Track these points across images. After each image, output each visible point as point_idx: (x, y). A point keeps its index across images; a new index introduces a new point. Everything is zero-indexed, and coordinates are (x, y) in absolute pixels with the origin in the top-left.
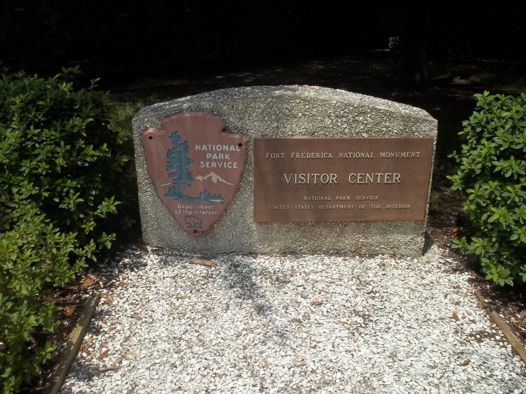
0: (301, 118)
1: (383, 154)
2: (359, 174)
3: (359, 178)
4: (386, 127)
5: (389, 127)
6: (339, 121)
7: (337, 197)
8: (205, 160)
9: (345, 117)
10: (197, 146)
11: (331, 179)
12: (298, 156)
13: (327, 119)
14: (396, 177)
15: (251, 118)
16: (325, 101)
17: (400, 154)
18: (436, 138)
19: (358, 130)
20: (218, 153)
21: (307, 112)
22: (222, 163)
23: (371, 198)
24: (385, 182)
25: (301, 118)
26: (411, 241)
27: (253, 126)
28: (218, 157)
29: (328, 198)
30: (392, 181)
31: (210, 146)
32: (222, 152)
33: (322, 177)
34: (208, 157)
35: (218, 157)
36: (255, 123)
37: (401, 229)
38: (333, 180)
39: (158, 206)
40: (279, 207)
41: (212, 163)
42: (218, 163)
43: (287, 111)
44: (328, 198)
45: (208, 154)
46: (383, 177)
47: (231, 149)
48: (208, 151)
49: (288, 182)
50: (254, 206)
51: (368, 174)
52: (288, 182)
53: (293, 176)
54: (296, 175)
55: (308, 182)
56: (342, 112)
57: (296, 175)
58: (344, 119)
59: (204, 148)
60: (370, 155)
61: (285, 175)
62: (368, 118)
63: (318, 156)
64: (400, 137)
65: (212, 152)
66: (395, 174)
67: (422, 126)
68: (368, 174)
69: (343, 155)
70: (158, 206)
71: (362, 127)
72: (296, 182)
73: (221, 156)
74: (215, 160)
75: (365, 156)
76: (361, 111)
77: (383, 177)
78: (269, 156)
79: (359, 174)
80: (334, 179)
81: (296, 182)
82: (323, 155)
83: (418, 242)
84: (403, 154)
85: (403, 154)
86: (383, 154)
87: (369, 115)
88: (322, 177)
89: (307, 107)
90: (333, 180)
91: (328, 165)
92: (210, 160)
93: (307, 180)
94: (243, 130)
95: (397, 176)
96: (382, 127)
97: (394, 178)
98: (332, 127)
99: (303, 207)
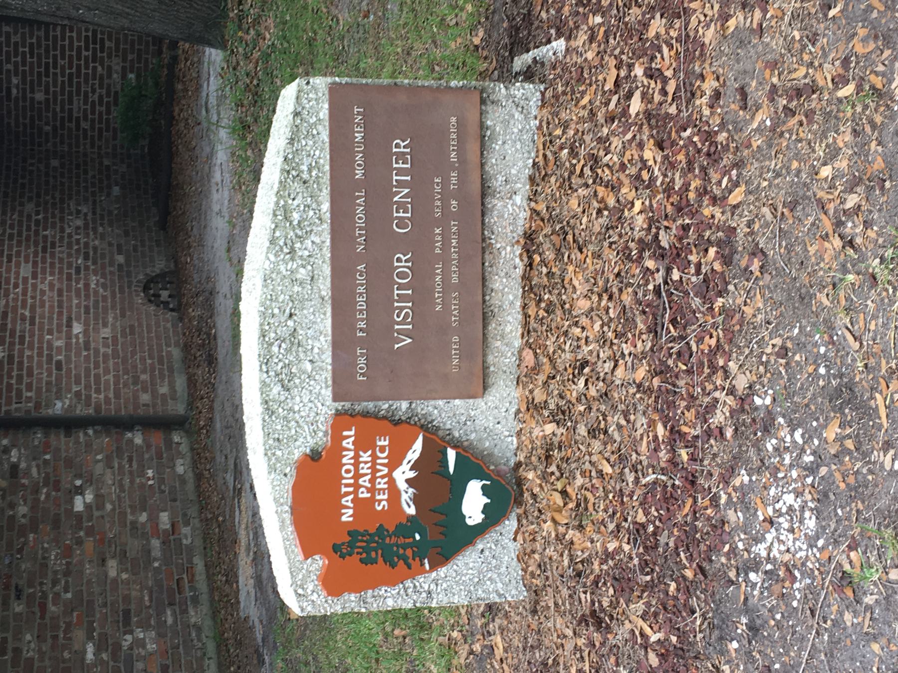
0: (295, 322)
1: (359, 173)
2: (395, 215)
3: (401, 215)
4: (310, 170)
5: (311, 165)
6: (300, 254)
7: (438, 251)
8: (372, 500)
9: (293, 244)
10: (344, 518)
11: (403, 264)
12: (362, 325)
13: (299, 276)
14: (400, 146)
15: (296, 408)
16: (265, 280)
17: (357, 142)
18: (329, 80)
19: (317, 221)
20: (357, 476)
21: (284, 311)
22: (378, 467)
23: (438, 189)
24: (409, 166)
25: (295, 322)
26: (520, 109)
27: (310, 405)
28: (367, 474)
29: (439, 268)
30: (407, 153)
31: (344, 490)
32: (356, 464)
33: (400, 281)
34: (367, 495)
35: (367, 474)
36: (306, 400)
37: (498, 129)
38: (406, 261)
39: (456, 571)
40: (455, 354)
41: (378, 487)
42: (378, 474)
43: (283, 345)
44: (439, 268)
45: (361, 496)
46: (400, 171)
47: (351, 446)
48: (355, 492)
49: (410, 340)
50: (455, 399)
51: (396, 199)
52: (410, 340)
53: (399, 332)
54: (397, 327)
55: (410, 304)
56: (285, 247)
57: (397, 327)
58: (298, 245)
59: (347, 501)
60: (361, 197)
61: (396, 346)
62: (296, 202)
63: (361, 289)
64: (327, 145)
65: (357, 486)
66: (394, 150)
67: (307, 106)
68: (396, 199)
69: (361, 244)
70: (456, 571)
71: (311, 213)
72: (410, 327)
73: (365, 469)
74: (372, 481)
75: (362, 206)
76: (282, 213)
77: (400, 171)
78: (363, 375)
79: (395, 215)
80: (404, 259)
81: (410, 327)
82: (361, 279)
83: (523, 94)
84: (359, 137)
85: (359, 137)
86: (359, 173)
87: (290, 202)
88: (400, 281)
89: (276, 311)
90: (406, 261)
91: (381, 275)
92: (372, 490)
93: (398, 323)
94: (317, 422)
95: (397, 146)
96: (311, 176)
97: (402, 150)
98: (312, 266)
99: (455, 312)
